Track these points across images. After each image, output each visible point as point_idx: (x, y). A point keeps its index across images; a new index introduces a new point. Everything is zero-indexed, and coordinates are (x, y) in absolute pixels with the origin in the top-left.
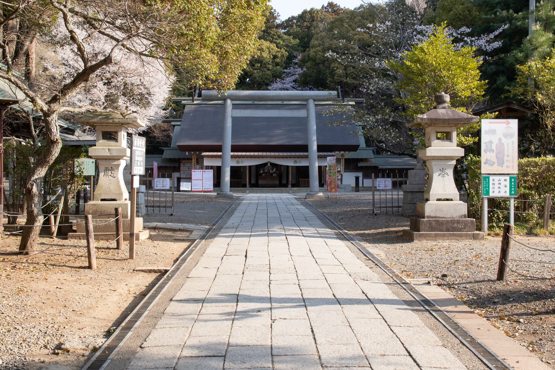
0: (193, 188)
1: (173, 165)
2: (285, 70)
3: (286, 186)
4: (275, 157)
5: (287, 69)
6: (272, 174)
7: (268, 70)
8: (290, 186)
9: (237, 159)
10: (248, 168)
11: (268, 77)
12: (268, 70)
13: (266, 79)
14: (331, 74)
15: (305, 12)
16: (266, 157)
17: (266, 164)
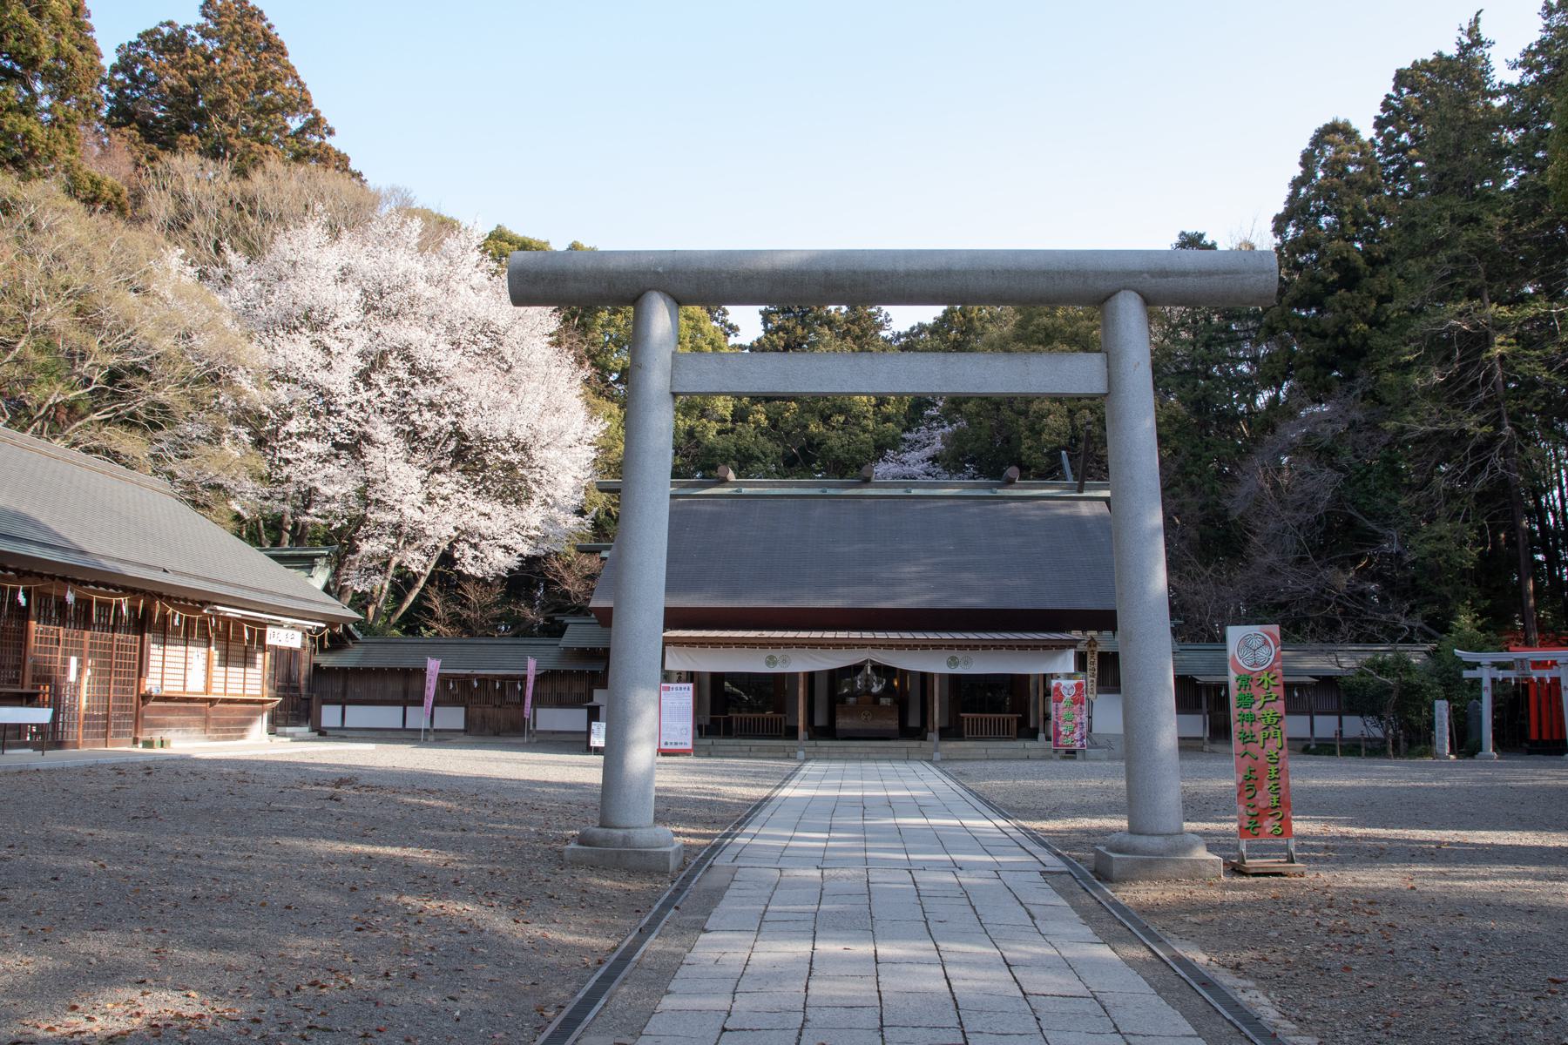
1: (588, 669)
2: (907, 435)
3: (919, 734)
4: (889, 646)
6: (876, 697)
7: (865, 431)
8: (933, 736)
9: (770, 652)
10: (801, 679)
11: (864, 447)
12: (865, 431)
13: (860, 452)
14: (1032, 429)
16: (861, 645)
17: (858, 668)
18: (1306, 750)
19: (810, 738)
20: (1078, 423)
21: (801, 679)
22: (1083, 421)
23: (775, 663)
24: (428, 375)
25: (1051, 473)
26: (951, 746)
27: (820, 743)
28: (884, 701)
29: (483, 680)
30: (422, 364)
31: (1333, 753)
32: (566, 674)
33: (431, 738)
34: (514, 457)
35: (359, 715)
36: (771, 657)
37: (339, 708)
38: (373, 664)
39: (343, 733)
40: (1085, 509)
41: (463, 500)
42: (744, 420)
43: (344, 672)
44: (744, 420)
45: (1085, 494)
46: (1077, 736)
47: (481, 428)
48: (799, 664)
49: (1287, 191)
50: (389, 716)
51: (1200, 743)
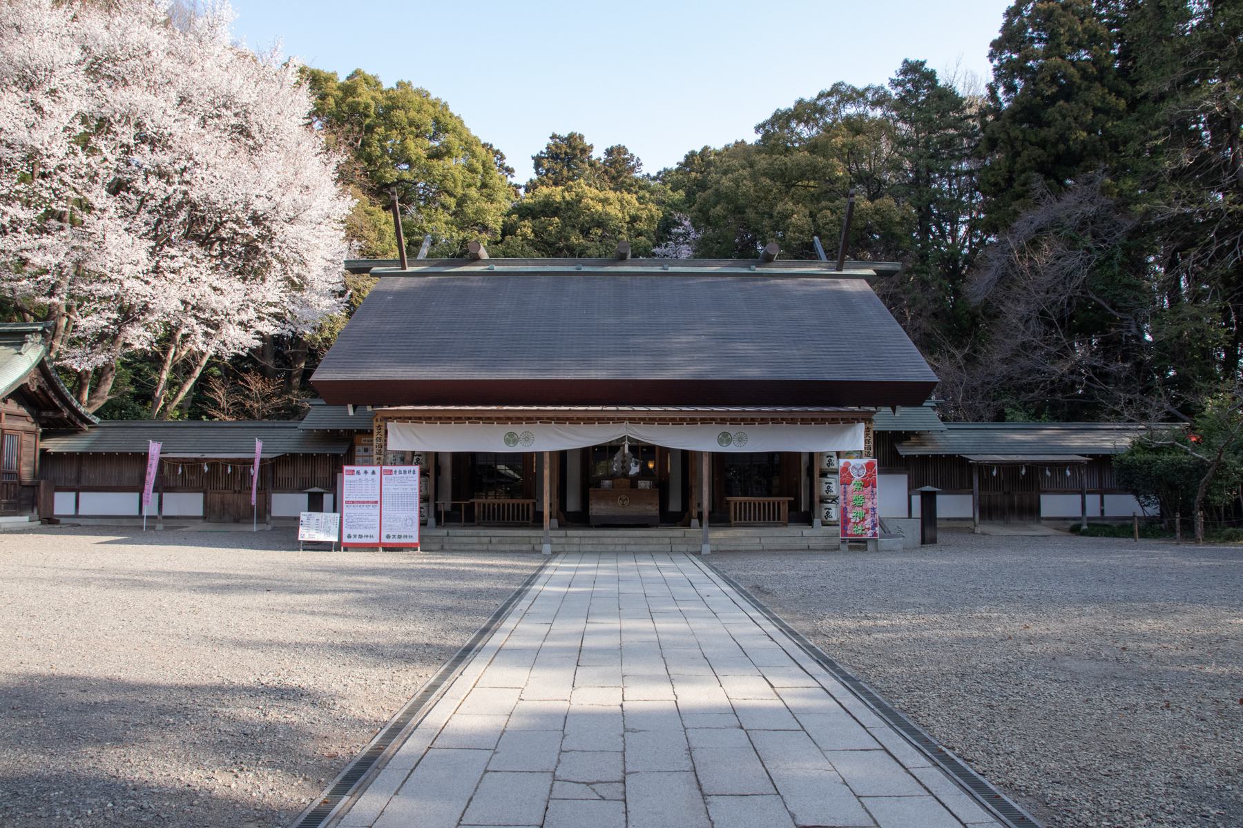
0: (346, 532)
2: (657, 250)
3: (680, 519)
5: (659, 246)
6: (634, 481)
9: (510, 427)
10: (547, 459)
15: (690, 157)
18: (1076, 530)
19: (562, 526)
20: (820, 222)
21: (547, 459)
22: (825, 221)
23: (515, 442)
24: (154, 142)
25: (805, 253)
26: (719, 535)
27: (571, 533)
28: (644, 484)
29: (214, 464)
30: (150, 129)
31: (1131, 534)
32: (307, 457)
33: (160, 526)
34: (254, 231)
35: (93, 503)
36: (725, 434)
37: (73, 495)
38: (103, 449)
39: (77, 521)
40: (847, 286)
41: (196, 275)
42: (513, 233)
43: (71, 456)
44: (513, 233)
45: (844, 272)
46: (868, 523)
47: (213, 197)
48: (546, 440)
49: (1001, 21)
50: (122, 503)
51: (970, 524)
